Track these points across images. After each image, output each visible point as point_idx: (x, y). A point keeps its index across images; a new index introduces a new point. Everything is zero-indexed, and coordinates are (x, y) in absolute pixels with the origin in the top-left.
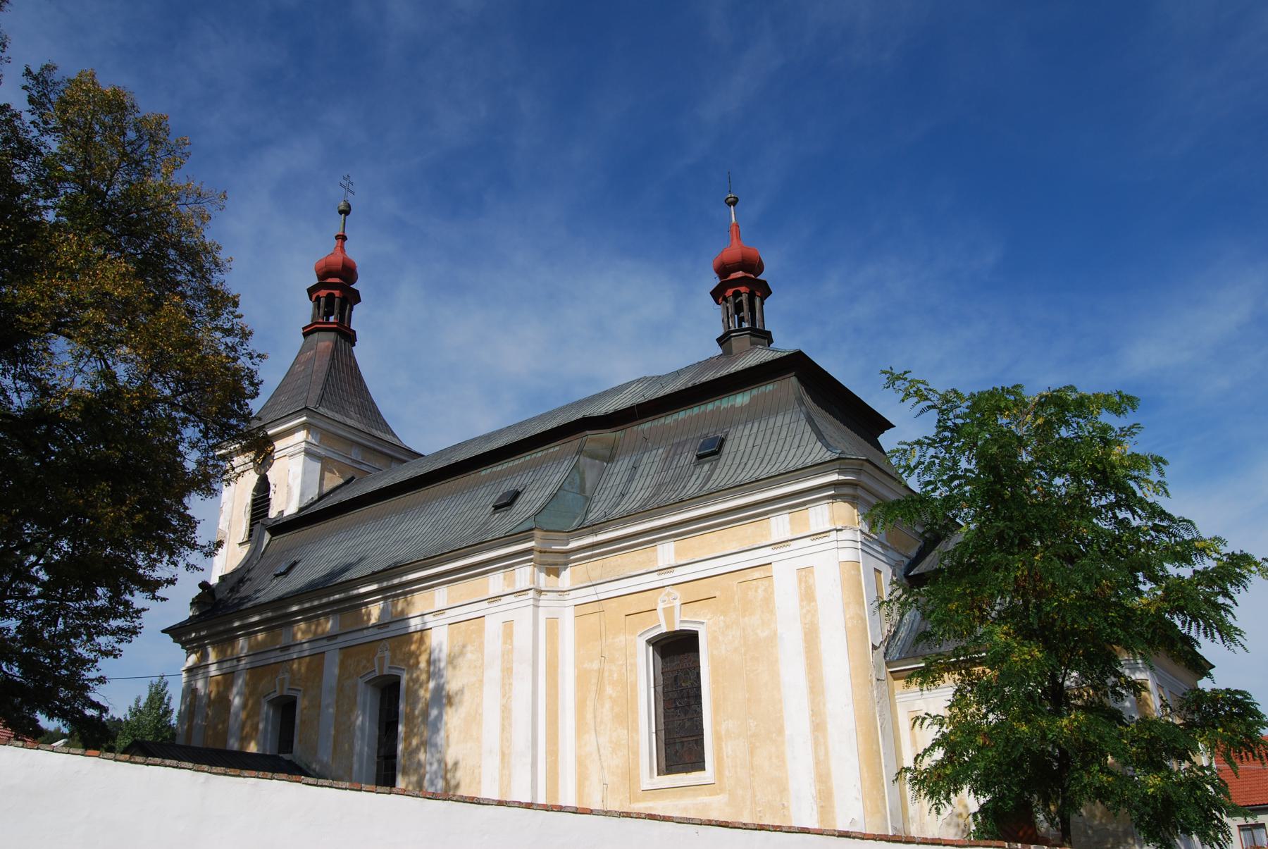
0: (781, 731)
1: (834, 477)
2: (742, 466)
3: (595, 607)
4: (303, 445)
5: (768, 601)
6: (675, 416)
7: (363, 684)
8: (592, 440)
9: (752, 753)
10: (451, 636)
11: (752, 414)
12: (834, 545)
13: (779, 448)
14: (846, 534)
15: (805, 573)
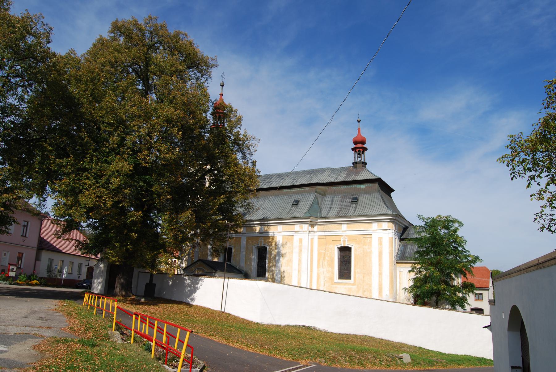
0: (371, 273)
1: (390, 217)
2: (364, 207)
3: (324, 237)
5: (370, 243)
6: (343, 187)
8: (319, 189)
9: (363, 278)
10: (283, 239)
11: (366, 192)
12: (388, 233)
13: (374, 205)
14: (391, 231)
15: (380, 239)
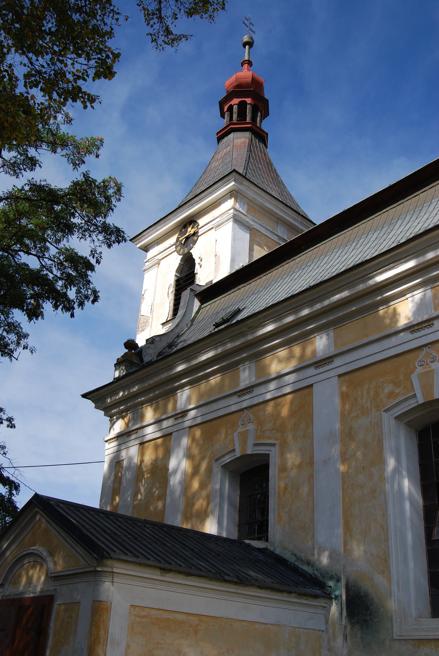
4: (232, 211)
7: (394, 419)
